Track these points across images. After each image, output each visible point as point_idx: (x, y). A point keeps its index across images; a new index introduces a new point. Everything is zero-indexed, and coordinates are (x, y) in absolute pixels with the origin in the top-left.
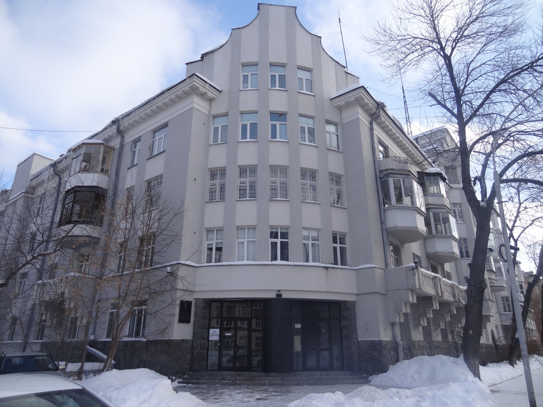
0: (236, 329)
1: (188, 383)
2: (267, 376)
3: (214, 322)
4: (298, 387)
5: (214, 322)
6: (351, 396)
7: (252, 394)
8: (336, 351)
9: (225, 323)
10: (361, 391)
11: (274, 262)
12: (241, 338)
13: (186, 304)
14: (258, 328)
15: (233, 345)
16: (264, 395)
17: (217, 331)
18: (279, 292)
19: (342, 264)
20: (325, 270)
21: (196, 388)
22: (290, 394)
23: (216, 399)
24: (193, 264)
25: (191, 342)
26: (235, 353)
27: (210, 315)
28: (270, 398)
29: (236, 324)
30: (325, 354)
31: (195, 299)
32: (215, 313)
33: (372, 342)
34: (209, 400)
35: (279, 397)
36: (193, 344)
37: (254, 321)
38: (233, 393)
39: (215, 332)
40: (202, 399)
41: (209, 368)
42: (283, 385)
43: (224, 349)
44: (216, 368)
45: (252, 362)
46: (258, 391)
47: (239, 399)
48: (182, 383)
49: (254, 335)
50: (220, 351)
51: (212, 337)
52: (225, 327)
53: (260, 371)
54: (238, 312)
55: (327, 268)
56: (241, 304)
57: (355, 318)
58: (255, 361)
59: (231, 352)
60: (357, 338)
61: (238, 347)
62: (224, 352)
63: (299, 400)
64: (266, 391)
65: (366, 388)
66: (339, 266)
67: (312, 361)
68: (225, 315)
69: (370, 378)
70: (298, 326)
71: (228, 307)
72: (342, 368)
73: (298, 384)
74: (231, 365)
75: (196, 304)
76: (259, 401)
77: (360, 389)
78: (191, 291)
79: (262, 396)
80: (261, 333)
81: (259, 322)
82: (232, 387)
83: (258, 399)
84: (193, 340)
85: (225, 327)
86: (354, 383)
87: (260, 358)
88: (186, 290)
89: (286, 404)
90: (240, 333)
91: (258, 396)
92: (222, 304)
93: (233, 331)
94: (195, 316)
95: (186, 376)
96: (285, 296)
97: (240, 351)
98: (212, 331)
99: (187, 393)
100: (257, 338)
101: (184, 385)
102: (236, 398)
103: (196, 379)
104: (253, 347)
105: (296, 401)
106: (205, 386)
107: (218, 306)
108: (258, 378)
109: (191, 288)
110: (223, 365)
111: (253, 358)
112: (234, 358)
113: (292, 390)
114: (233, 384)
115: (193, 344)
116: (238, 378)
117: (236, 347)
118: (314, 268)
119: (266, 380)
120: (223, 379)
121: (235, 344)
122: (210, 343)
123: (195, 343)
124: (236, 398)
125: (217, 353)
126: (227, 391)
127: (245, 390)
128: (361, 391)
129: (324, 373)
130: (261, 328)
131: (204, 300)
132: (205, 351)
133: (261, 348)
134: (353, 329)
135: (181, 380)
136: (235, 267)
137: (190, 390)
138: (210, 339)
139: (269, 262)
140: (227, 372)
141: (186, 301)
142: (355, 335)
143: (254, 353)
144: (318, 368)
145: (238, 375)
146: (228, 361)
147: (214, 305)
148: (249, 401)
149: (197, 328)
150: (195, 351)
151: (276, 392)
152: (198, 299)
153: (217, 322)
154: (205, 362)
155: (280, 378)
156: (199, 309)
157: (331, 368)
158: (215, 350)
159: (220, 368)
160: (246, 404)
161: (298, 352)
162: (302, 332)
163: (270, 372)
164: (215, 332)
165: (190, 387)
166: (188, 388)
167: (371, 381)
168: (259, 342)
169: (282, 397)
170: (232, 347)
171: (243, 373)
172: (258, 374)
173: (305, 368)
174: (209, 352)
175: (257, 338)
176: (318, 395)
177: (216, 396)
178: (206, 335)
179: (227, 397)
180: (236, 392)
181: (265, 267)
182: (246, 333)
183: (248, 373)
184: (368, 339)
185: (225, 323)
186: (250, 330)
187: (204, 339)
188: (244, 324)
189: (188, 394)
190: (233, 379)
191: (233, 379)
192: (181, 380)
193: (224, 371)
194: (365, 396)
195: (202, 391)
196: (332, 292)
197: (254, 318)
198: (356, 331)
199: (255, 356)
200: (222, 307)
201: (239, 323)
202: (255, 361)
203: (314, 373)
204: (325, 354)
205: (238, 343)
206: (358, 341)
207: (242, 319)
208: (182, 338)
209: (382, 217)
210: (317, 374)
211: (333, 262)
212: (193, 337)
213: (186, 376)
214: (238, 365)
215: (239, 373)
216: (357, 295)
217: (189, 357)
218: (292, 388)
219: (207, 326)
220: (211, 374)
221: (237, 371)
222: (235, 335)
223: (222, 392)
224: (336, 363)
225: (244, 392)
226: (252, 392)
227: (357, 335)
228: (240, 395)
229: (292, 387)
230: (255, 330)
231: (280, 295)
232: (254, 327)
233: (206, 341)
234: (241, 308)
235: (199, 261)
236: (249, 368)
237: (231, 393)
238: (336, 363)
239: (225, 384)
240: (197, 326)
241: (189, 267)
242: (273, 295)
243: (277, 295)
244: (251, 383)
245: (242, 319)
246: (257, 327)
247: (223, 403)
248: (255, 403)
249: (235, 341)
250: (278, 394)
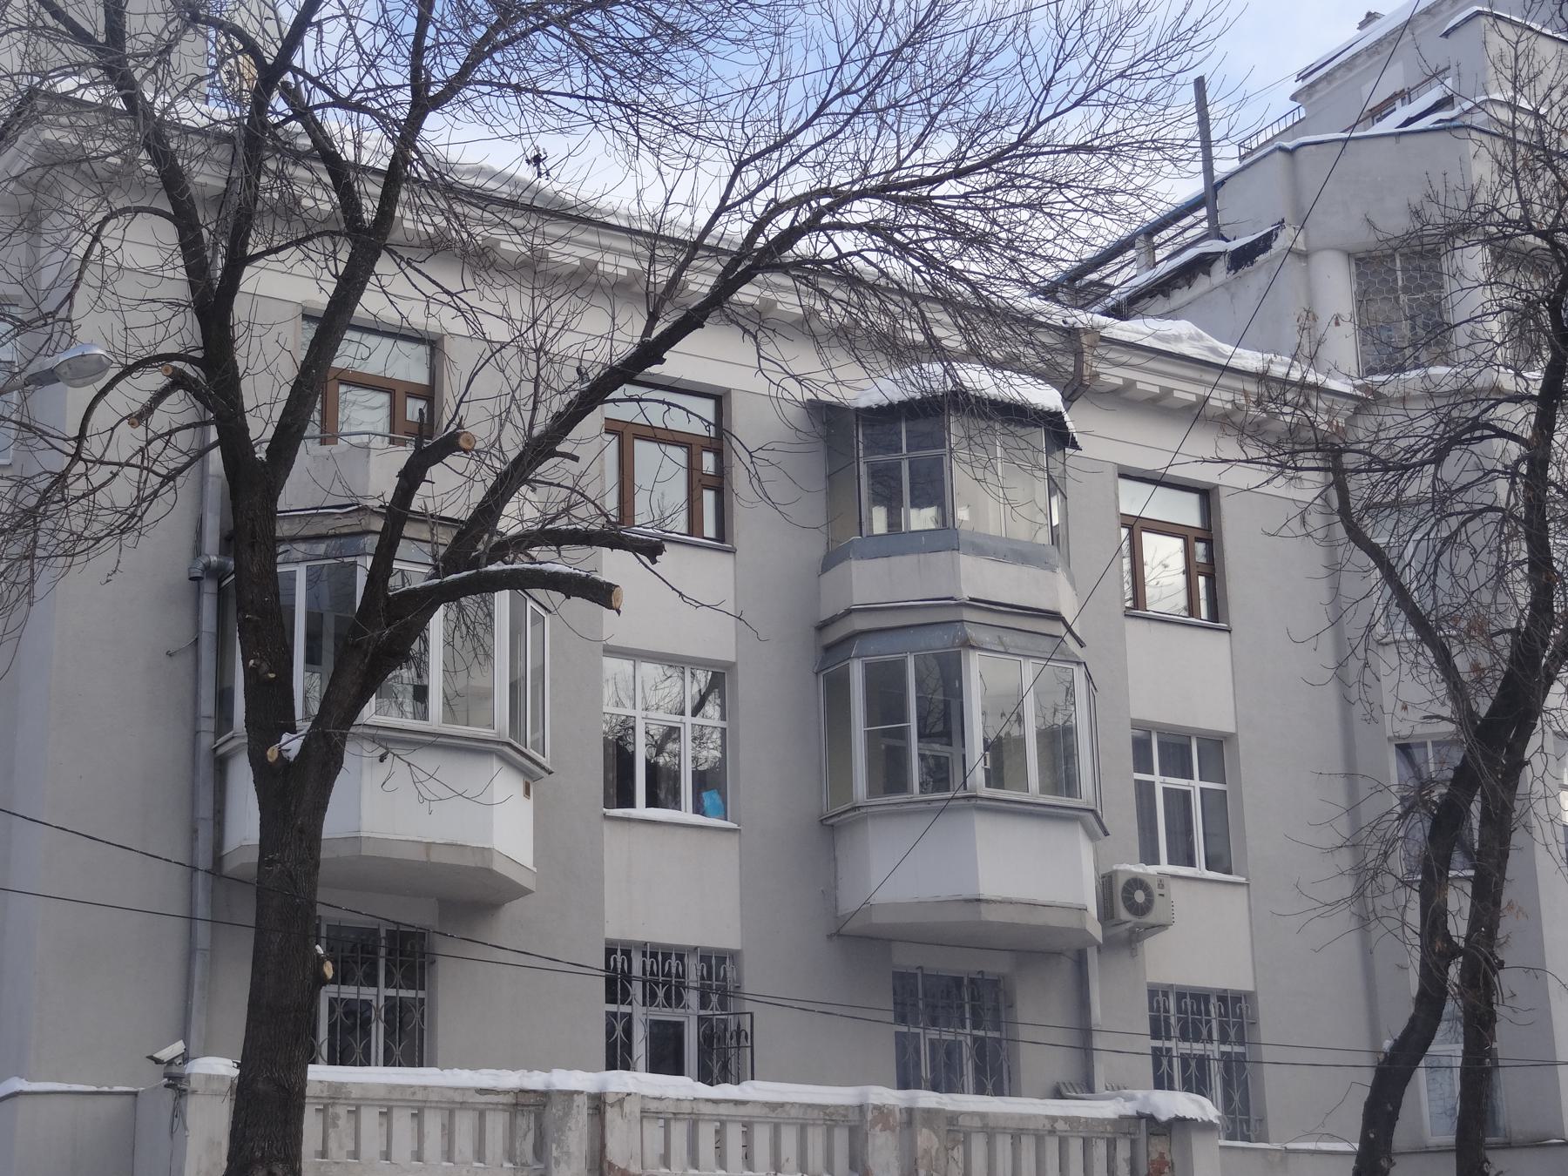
209: (205, 810)
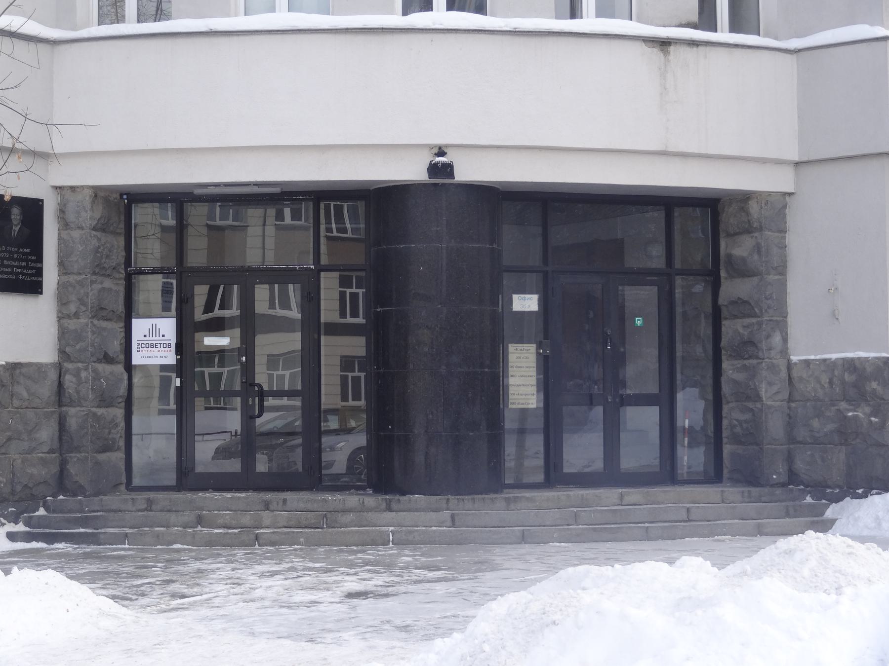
0: (249, 325)
1: (50, 539)
2: (389, 509)
3: (150, 288)
4: (525, 548)
5: (150, 288)
6: (744, 573)
7: (326, 577)
8: (690, 408)
9: (201, 293)
10: (789, 553)
11: (419, 19)
12: (273, 361)
13: (16, 212)
14: (350, 320)
15: (238, 387)
16: (377, 581)
17: (168, 327)
18: (441, 153)
19: (736, 26)
20: (654, 53)
21: (87, 556)
22: (488, 575)
23: (174, 596)
24: (32, 28)
25: (53, 375)
26: (249, 418)
27: (128, 262)
28: (402, 588)
29: (247, 302)
30: (643, 420)
31: (58, 189)
32: (151, 250)
33: (851, 365)
34: (144, 601)
35: (440, 588)
36: (60, 385)
37: (329, 284)
38: (246, 573)
39: (154, 331)
40: (114, 597)
41: (137, 481)
42: (459, 543)
43: (199, 402)
44: (171, 479)
45: (326, 457)
46: (351, 565)
47: (271, 594)
48: (28, 537)
49: (333, 349)
50: (184, 413)
51: (145, 352)
52: (199, 316)
53: (358, 488)
54: (259, 242)
55: (664, 44)
56: (271, 212)
57: (782, 270)
58: (340, 451)
59: (233, 420)
60: (785, 352)
61: (262, 394)
62: (203, 419)
63: (523, 593)
64: (389, 566)
65: (810, 541)
66: (723, 35)
67: (583, 450)
68: (197, 257)
69: (829, 513)
70: (526, 303)
71: (209, 227)
72: (714, 474)
73: (523, 539)
74: (234, 466)
75: (62, 211)
76: (355, 601)
77: (784, 543)
78: (34, 154)
79: (369, 586)
80: (361, 341)
81: (354, 296)
82: (240, 553)
83: (351, 595)
84: (59, 368)
85: (199, 316)
86: (760, 531)
87: (361, 440)
88: (12, 151)
89: (470, 613)
90: (267, 344)
91: (352, 584)
92: (180, 216)
93: (237, 332)
94: (61, 264)
95: (42, 512)
96: (469, 171)
97: (267, 416)
98: (140, 327)
99: (50, 573)
100: (347, 363)
101: (35, 545)
102: (258, 593)
103: (84, 522)
104: (330, 395)
105: (512, 597)
106: (124, 549)
107: (164, 229)
108: (351, 517)
109: (32, 139)
110: (199, 469)
111: (326, 440)
112: (248, 442)
113: (498, 560)
114: (248, 539)
115: (60, 385)
116: (267, 517)
117: (253, 395)
118: (604, 42)
119: (388, 522)
120: (200, 521)
121: (249, 383)
122: (136, 380)
123: (69, 380)
124: (258, 593)
125: (170, 423)
126: (220, 568)
127: (298, 563)
128: (789, 553)
129: (634, 494)
130: (361, 320)
131: (100, 194)
132: (119, 413)
133: (362, 403)
134: (770, 311)
135: (21, 527)
136: (235, 39)
137: (63, 564)
138: (137, 359)
139: (397, 20)
140: (217, 496)
141: (16, 200)
142: (777, 339)
143: (333, 423)
144: (612, 475)
145: (267, 506)
146: (222, 453)
147: (142, 214)
148: (314, 603)
149: (76, 315)
150: (72, 411)
151: (428, 568)
152: (73, 188)
153: (166, 291)
154: (118, 457)
155: (447, 514)
156: (76, 234)
157: (667, 473)
158: (162, 412)
159: (187, 477)
160: (303, 613)
161: (524, 413)
162: (545, 328)
163: (404, 493)
164: (154, 331)
165: (60, 556)
166: (51, 557)
167: (833, 522)
168: (356, 380)
169: (452, 587)
170: (235, 394)
171: (288, 495)
172: (352, 500)
173: (554, 475)
174: (136, 420)
175: (347, 363)
176: (606, 571)
177: (172, 587)
178: (115, 347)
179: (221, 588)
180: (260, 568)
181: (373, 40)
182: (293, 341)
183: (306, 495)
184: (834, 356)
185: (201, 293)
186: (313, 328)
187: (107, 359)
188: (286, 305)
189: (52, 577)
190: (246, 519)
191: (246, 519)
192: (21, 527)
193: (205, 489)
194: (806, 572)
195: (112, 567)
196: (684, 155)
197: (329, 269)
198: (781, 324)
199: (336, 432)
200: (181, 227)
201: (262, 293)
202: (340, 451)
203: (588, 493)
204: (643, 420)
205: (261, 377)
206: (790, 366)
207: (276, 276)
208: (13, 359)
210: (608, 497)
211: (695, 17)
212: (62, 352)
213: (42, 512)
214: (262, 465)
215: (268, 496)
216: (797, 164)
217: (47, 433)
218: (498, 554)
219: (121, 308)
220: (150, 502)
221: (258, 489)
222: (247, 347)
223: (199, 571)
224: (690, 457)
225: (293, 569)
226: (326, 571)
227: (785, 340)
228: (277, 583)
229: (497, 550)
230: (334, 329)
231: (446, 170)
232: (329, 312)
233: (120, 369)
234: (270, 230)
235: (63, 13)
236: (312, 477)
237: (238, 574)
238: (690, 457)
239: (211, 542)
240: (73, 308)
241: (20, 44)
242: (412, 170)
243: (435, 170)
244: (320, 536)
245: (276, 276)
246: (343, 315)
247: (204, 612)
248: (343, 608)
249: (248, 369)
250: (440, 574)
